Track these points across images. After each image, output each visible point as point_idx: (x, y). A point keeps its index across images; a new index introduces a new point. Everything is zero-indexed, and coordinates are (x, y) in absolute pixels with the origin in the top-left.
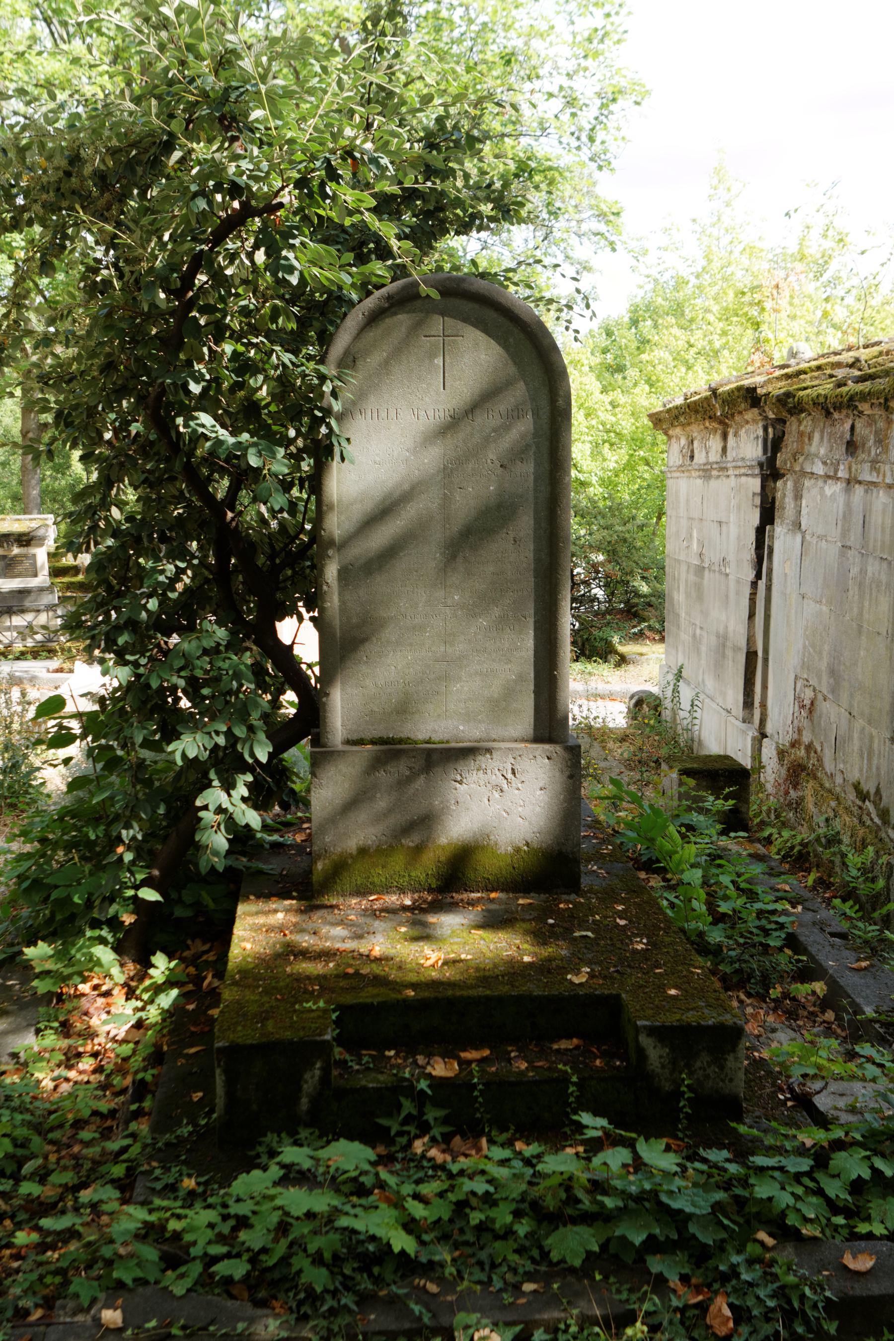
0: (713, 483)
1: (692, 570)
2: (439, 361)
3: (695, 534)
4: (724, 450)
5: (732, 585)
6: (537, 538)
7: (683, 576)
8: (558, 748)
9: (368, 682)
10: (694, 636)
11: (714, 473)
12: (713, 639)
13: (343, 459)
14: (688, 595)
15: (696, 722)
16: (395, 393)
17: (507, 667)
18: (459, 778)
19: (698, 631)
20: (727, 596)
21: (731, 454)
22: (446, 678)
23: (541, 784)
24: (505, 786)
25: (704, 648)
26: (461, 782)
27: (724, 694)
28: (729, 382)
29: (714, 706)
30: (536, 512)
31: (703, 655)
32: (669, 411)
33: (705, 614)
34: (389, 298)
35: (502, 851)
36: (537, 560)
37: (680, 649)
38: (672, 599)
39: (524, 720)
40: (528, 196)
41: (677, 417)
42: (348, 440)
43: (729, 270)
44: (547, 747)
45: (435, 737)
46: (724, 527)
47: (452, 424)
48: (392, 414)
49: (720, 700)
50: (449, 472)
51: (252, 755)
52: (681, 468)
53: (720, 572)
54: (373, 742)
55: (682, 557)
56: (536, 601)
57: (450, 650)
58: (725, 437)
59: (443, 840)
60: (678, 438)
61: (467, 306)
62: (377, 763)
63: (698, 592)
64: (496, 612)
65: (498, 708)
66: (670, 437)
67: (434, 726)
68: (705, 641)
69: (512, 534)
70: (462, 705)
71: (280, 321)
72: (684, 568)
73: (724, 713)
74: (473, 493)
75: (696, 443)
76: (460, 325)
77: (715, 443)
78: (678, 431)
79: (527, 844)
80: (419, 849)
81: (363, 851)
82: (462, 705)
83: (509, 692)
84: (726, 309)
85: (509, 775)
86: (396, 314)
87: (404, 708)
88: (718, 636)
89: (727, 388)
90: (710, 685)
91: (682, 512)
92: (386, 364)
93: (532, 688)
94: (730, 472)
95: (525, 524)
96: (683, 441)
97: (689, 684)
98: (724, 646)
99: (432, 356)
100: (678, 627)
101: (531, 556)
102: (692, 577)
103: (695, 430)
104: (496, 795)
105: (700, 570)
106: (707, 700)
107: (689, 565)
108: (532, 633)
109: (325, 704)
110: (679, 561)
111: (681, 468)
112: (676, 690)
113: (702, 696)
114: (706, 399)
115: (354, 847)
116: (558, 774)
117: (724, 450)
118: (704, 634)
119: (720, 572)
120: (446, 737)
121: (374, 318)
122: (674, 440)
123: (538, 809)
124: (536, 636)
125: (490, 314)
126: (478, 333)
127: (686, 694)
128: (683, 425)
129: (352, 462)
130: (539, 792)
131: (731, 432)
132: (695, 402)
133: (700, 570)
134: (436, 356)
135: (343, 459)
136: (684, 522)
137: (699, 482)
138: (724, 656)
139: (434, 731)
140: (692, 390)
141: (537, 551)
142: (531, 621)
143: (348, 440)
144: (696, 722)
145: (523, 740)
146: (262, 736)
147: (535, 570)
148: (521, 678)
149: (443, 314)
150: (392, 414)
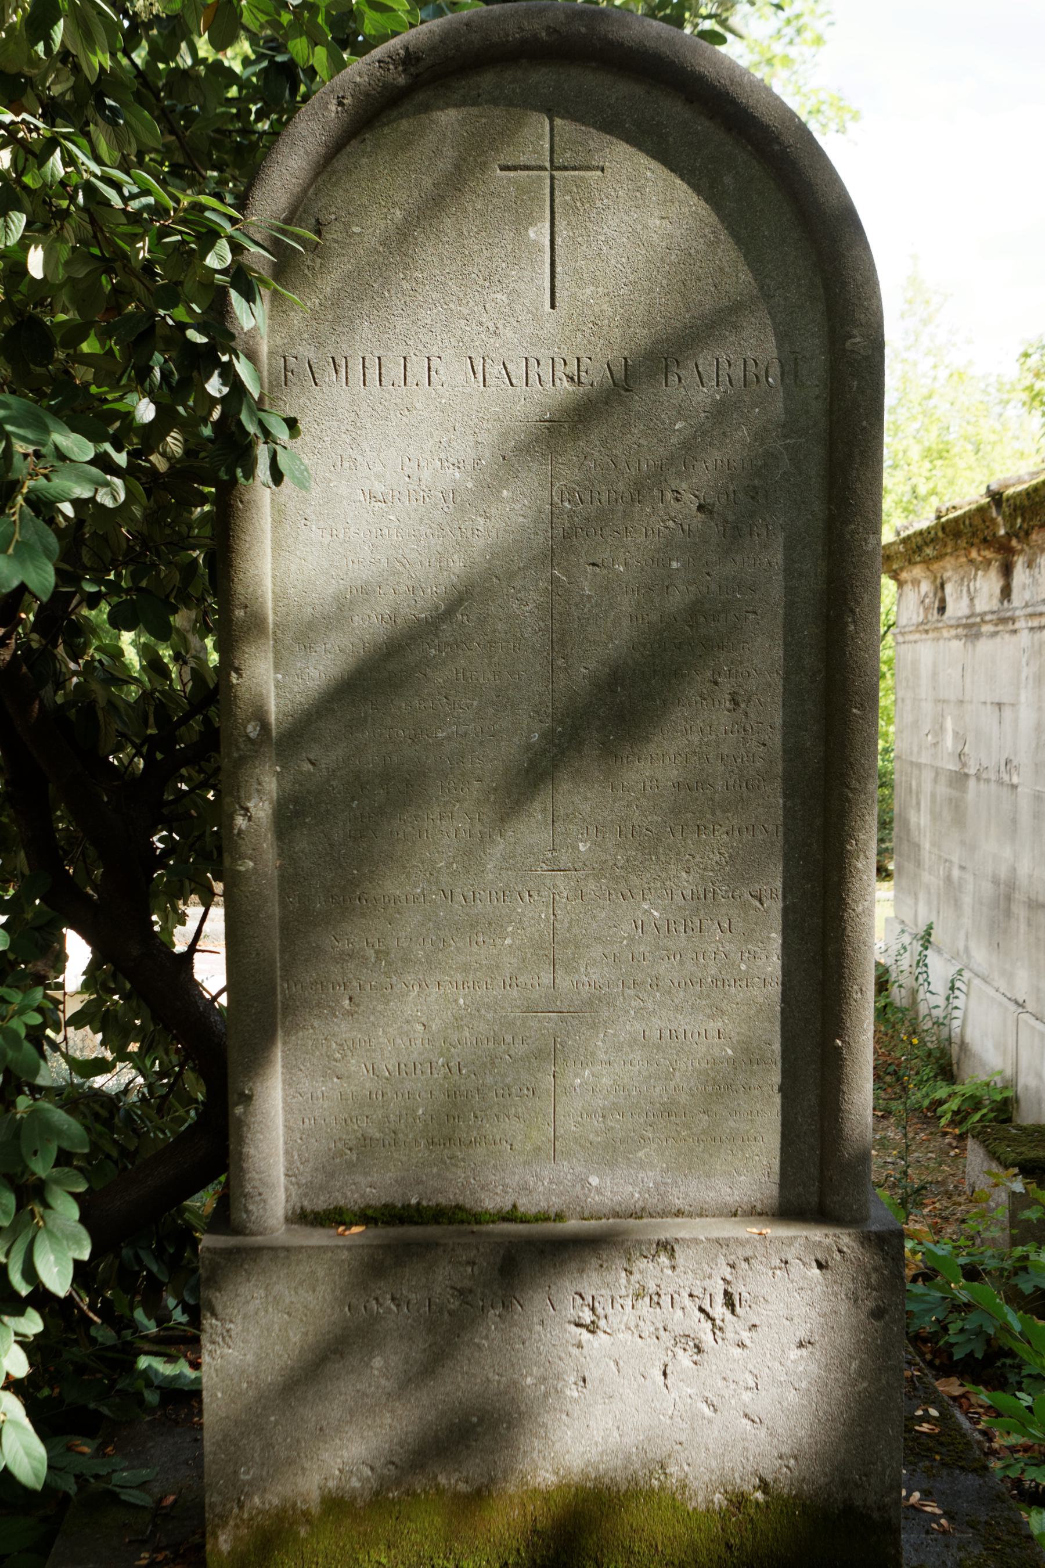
0: (984, 646)
1: (943, 780)
2: (539, 233)
3: (949, 724)
4: (1006, 592)
5: (1025, 804)
6: (792, 696)
7: (927, 787)
8: (846, 1239)
9: (355, 1065)
10: (948, 879)
11: (986, 628)
12: (987, 887)
13: (277, 476)
14: (935, 816)
15: (956, 1013)
16: (426, 316)
17: (713, 1026)
18: (587, 1317)
19: (956, 873)
20: (1014, 821)
21: (1018, 597)
22: (552, 1053)
23: (802, 1334)
24: (707, 1338)
25: (967, 900)
26: (592, 1328)
27: (1010, 977)
28: (1020, 481)
29: (992, 992)
30: (790, 627)
31: (967, 910)
32: (905, 541)
33: (971, 847)
34: (409, 59)
35: (699, 1502)
36: (792, 752)
37: (922, 896)
38: (906, 823)
39: (754, 1165)
40: (734, 21)
41: (919, 549)
42: (292, 424)
43: (932, 402)
44: (817, 1234)
45: (527, 1205)
46: (1007, 712)
47: (575, 421)
48: (418, 369)
49: (1002, 984)
50: (564, 539)
51: (30, 1273)
52: (923, 628)
53: (1000, 782)
54: (367, 1217)
55: (925, 759)
56: (787, 858)
57: (565, 982)
58: (1007, 571)
59: (545, 1477)
60: (916, 583)
61: (618, 90)
62: (376, 1268)
63: (957, 813)
64: (687, 882)
65: (691, 1120)
66: (901, 584)
67: (530, 1174)
68: (970, 887)
69: (727, 685)
70: (597, 1123)
71: (58, 32)
72: (928, 776)
73: (1012, 1007)
74: (625, 579)
75: (949, 588)
76: (596, 138)
77: (988, 584)
78: (918, 571)
79: (764, 1486)
80: (478, 1497)
81: (336, 1505)
82: (597, 1123)
83: (719, 1087)
84: (929, 449)
85: (719, 1310)
86: (426, 108)
87: (454, 1115)
88: (996, 882)
89: (1020, 488)
90: (980, 956)
91: (924, 690)
92: (402, 240)
93: (776, 1078)
94: (1021, 624)
95: (761, 659)
96: (925, 587)
97: (939, 951)
98: (1009, 899)
99: (523, 220)
100: (918, 864)
101: (776, 739)
102: (943, 790)
103: (948, 568)
104: (685, 1359)
105: (960, 779)
106: (976, 982)
107: (937, 772)
108: (776, 938)
109: (240, 1123)
110: (919, 766)
111: (923, 628)
112: (921, 962)
113: (967, 974)
114: (981, 510)
115: (315, 1495)
116: (843, 1307)
117: (1006, 592)
118: (969, 877)
119: (1000, 782)
120: (556, 1203)
121: (373, 115)
122: (908, 588)
123: (792, 1396)
124: (785, 946)
125: (673, 110)
126: (643, 160)
127: (939, 970)
128: (927, 561)
129: (302, 484)
130: (794, 1353)
131: (1020, 562)
132: (956, 520)
133: (960, 779)
134: (531, 221)
135: (277, 476)
136: (927, 707)
137: (957, 644)
138: (1008, 913)
139: (525, 1188)
140: (948, 505)
141: (790, 728)
142: (775, 907)
143: (292, 424)
144: (956, 1013)
145: (754, 1213)
146: (66, 1211)
147: (788, 778)
148: (749, 1056)
149: (551, 113)
150: (418, 369)
